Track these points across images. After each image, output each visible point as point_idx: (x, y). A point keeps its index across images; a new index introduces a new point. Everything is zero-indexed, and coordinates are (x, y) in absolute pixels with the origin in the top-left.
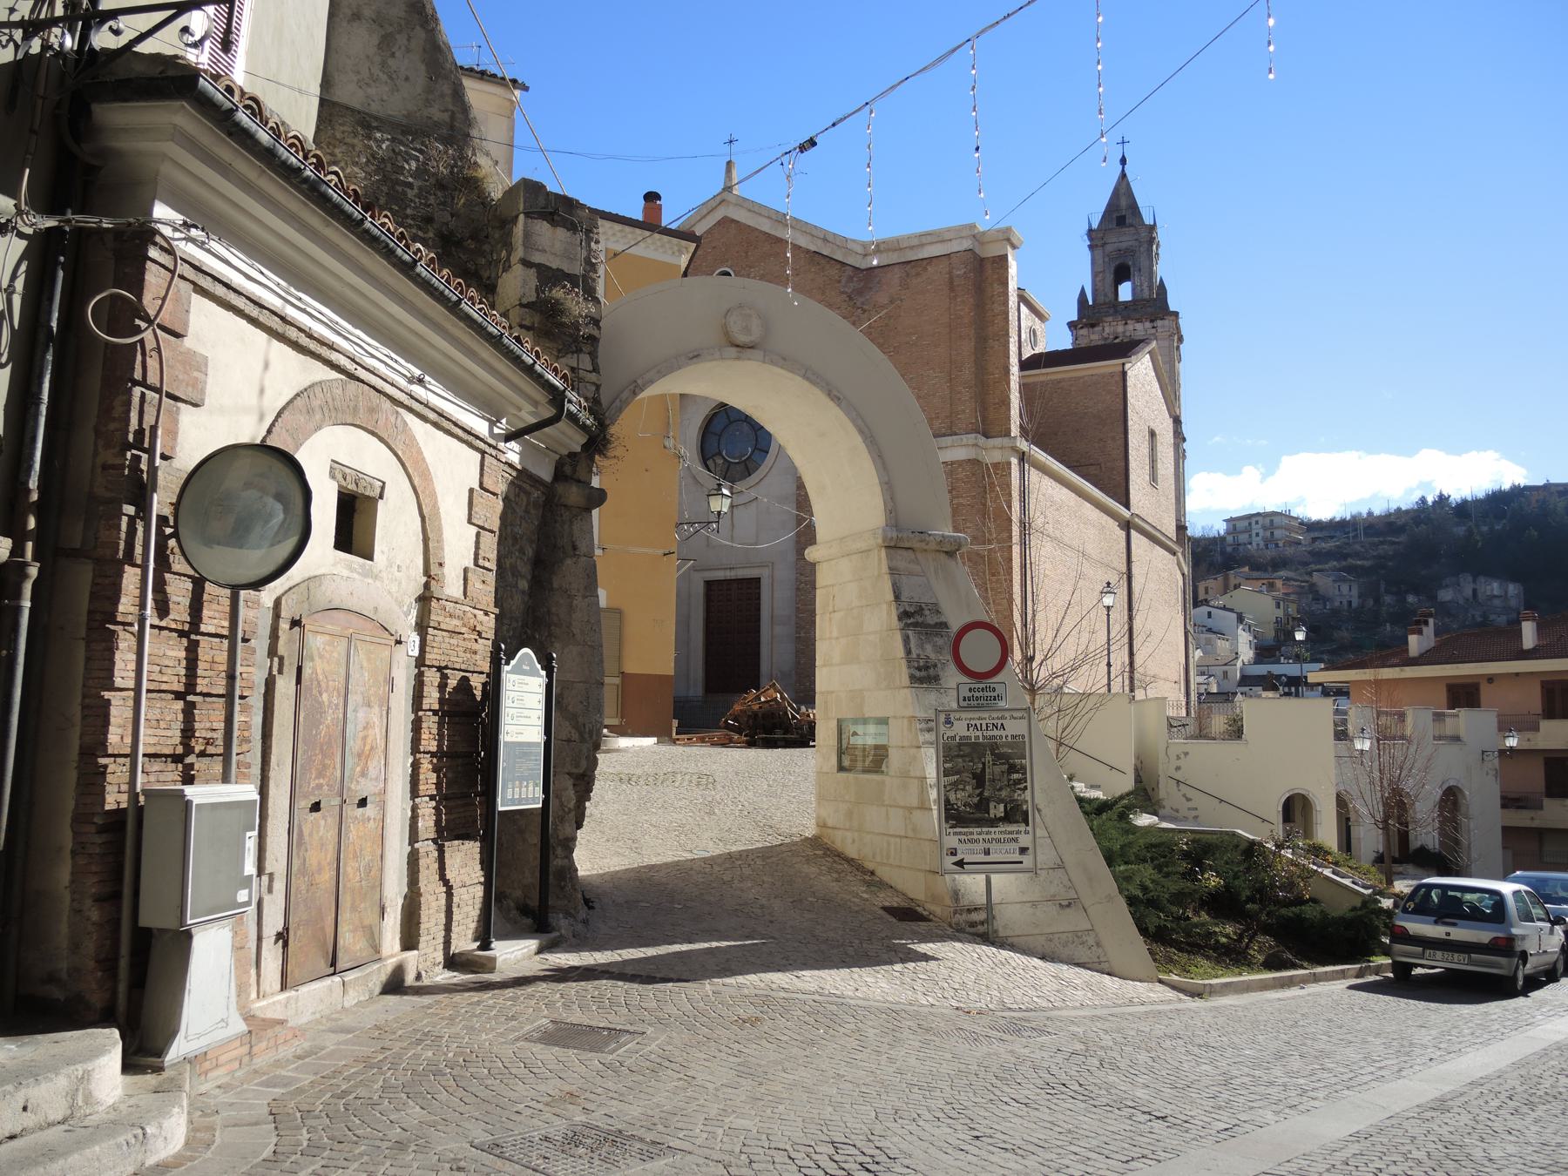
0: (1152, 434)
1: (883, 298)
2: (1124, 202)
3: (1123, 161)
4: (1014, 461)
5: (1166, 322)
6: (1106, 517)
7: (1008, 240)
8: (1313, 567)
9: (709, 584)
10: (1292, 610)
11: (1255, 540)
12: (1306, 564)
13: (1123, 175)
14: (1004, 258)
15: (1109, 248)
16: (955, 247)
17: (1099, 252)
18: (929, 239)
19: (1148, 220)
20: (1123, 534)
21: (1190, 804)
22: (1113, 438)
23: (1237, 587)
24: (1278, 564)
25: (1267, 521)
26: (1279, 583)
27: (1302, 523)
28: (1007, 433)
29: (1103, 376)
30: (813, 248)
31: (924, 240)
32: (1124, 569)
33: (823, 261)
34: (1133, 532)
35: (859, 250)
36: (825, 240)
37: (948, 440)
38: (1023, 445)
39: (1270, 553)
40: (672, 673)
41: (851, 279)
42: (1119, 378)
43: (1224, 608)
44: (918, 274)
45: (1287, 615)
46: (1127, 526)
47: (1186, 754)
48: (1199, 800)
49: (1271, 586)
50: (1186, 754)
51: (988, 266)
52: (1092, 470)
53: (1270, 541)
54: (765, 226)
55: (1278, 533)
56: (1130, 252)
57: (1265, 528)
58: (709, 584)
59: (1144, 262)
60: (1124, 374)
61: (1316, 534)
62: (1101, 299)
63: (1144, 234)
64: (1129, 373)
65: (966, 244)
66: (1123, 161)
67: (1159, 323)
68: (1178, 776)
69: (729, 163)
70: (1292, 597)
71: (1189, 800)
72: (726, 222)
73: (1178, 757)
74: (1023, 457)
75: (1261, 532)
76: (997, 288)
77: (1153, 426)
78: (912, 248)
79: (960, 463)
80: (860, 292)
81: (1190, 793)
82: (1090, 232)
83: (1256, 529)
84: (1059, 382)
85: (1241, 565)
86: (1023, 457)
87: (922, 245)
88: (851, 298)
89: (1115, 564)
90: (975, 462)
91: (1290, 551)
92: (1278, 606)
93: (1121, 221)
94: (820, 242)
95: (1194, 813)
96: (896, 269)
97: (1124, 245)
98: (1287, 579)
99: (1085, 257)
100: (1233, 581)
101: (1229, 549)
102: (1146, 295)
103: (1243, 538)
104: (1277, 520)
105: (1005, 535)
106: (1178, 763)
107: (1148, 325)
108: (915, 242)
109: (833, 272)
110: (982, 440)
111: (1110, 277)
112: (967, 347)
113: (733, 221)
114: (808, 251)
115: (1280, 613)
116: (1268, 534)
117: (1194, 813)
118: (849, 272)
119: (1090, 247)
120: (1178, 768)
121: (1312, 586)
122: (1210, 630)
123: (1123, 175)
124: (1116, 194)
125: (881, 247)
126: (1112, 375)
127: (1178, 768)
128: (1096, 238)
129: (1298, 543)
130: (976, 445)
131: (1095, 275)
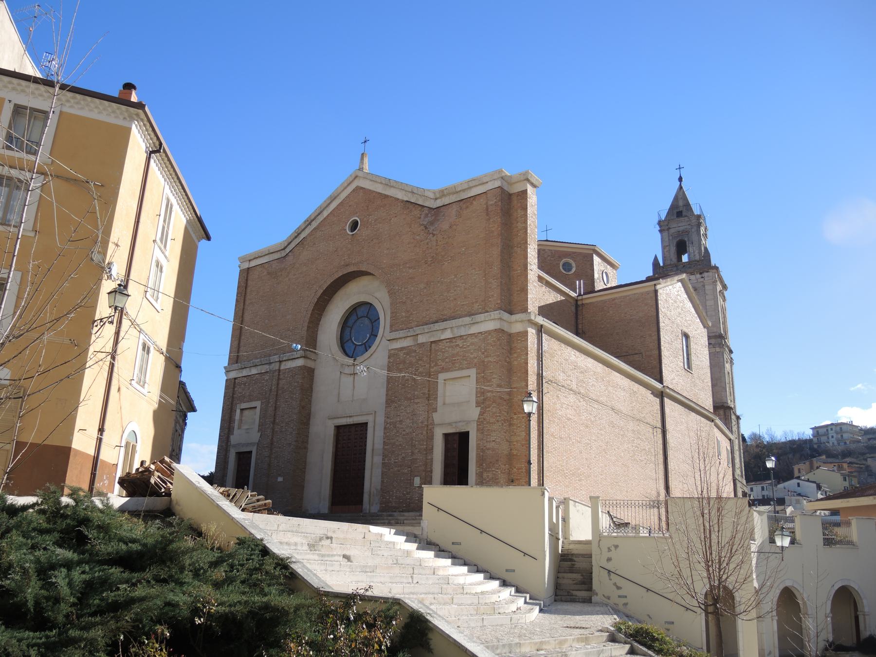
0: (686, 336)
1: (445, 226)
2: (681, 203)
3: (680, 179)
4: (532, 332)
5: (710, 274)
6: (637, 386)
7: (528, 180)
8: (868, 455)
9: (338, 428)
10: (855, 482)
11: (832, 440)
12: (863, 454)
13: (681, 187)
14: (525, 192)
15: (672, 231)
16: (490, 186)
17: (666, 234)
18: (474, 183)
19: (696, 212)
20: (658, 400)
21: (621, 592)
22: (650, 336)
23: (818, 468)
24: (846, 454)
25: (838, 428)
26: (845, 466)
27: (861, 430)
28: (525, 310)
29: (642, 294)
30: (406, 199)
31: (471, 184)
32: (659, 425)
33: (411, 206)
34: (666, 400)
35: (431, 195)
36: (413, 192)
37: (481, 317)
38: (541, 320)
39: (840, 448)
40: (590, 538)
41: (427, 215)
42: (653, 295)
43: (808, 481)
44: (467, 207)
45: (851, 485)
46: (661, 395)
47: (616, 547)
48: (628, 589)
49: (840, 468)
50: (616, 547)
51: (514, 198)
52: (637, 357)
53: (841, 440)
54: (379, 189)
55: (845, 436)
56: (686, 232)
57: (837, 433)
58: (338, 428)
59: (694, 237)
60: (656, 291)
61: (871, 436)
62: (668, 262)
63: (694, 221)
64: (660, 291)
65: (497, 184)
66: (680, 179)
67: (705, 274)
68: (609, 566)
69: (363, 154)
70: (855, 474)
71: (619, 588)
72: (358, 189)
73: (609, 550)
74: (540, 329)
75: (835, 435)
76: (520, 212)
77: (685, 330)
78: (464, 190)
79: (489, 332)
80: (432, 223)
81: (620, 582)
82: (660, 223)
83: (831, 433)
84: (614, 300)
85: (820, 455)
86: (540, 329)
87: (470, 188)
88: (426, 228)
89: (649, 420)
90: (501, 331)
91: (853, 446)
92: (845, 480)
93: (679, 214)
94: (410, 194)
95: (624, 600)
96: (454, 206)
97: (681, 229)
98: (850, 463)
99: (658, 236)
100: (816, 465)
101: (815, 446)
102: (697, 258)
103: (824, 439)
104: (844, 428)
105: (524, 384)
106: (609, 555)
107: (698, 276)
108: (466, 186)
109: (416, 212)
110: (506, 316)
111: (673, 249)
112: (496, 251)
113: (362, 188)
114: (403, 201)
115: (847, 484)
116: (839, 436)
117: (624, 600)
118: (426, 211)
119: (660, 231)
120: (609, 560)
121: (868, 466)
122: (799, 495)
123: (681, 187)
124: (676, 198)
125: (443, 193)
126: (648, 293)
127: (609, 560)
128: (664, 226)
129: (859, 441)
130: (501, 319)
131: (664, 248)
